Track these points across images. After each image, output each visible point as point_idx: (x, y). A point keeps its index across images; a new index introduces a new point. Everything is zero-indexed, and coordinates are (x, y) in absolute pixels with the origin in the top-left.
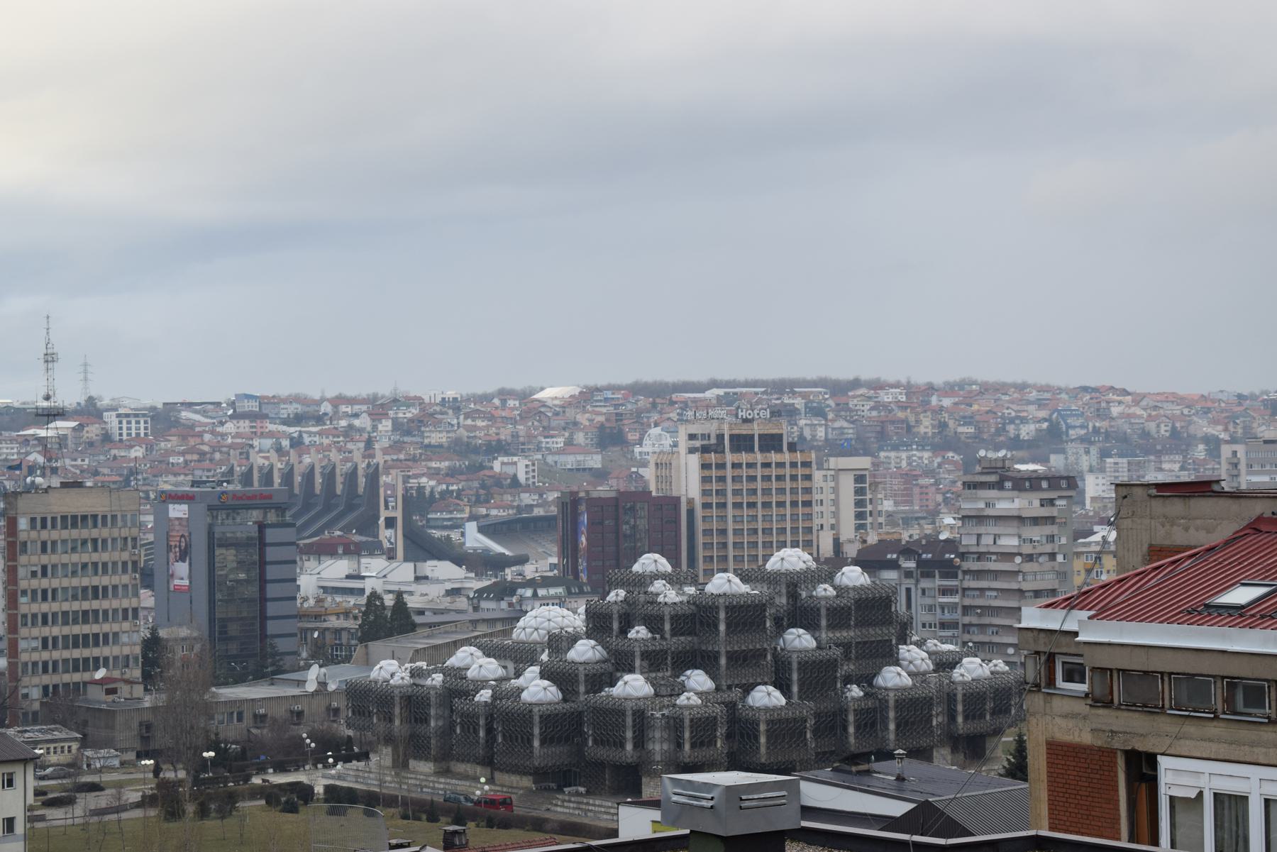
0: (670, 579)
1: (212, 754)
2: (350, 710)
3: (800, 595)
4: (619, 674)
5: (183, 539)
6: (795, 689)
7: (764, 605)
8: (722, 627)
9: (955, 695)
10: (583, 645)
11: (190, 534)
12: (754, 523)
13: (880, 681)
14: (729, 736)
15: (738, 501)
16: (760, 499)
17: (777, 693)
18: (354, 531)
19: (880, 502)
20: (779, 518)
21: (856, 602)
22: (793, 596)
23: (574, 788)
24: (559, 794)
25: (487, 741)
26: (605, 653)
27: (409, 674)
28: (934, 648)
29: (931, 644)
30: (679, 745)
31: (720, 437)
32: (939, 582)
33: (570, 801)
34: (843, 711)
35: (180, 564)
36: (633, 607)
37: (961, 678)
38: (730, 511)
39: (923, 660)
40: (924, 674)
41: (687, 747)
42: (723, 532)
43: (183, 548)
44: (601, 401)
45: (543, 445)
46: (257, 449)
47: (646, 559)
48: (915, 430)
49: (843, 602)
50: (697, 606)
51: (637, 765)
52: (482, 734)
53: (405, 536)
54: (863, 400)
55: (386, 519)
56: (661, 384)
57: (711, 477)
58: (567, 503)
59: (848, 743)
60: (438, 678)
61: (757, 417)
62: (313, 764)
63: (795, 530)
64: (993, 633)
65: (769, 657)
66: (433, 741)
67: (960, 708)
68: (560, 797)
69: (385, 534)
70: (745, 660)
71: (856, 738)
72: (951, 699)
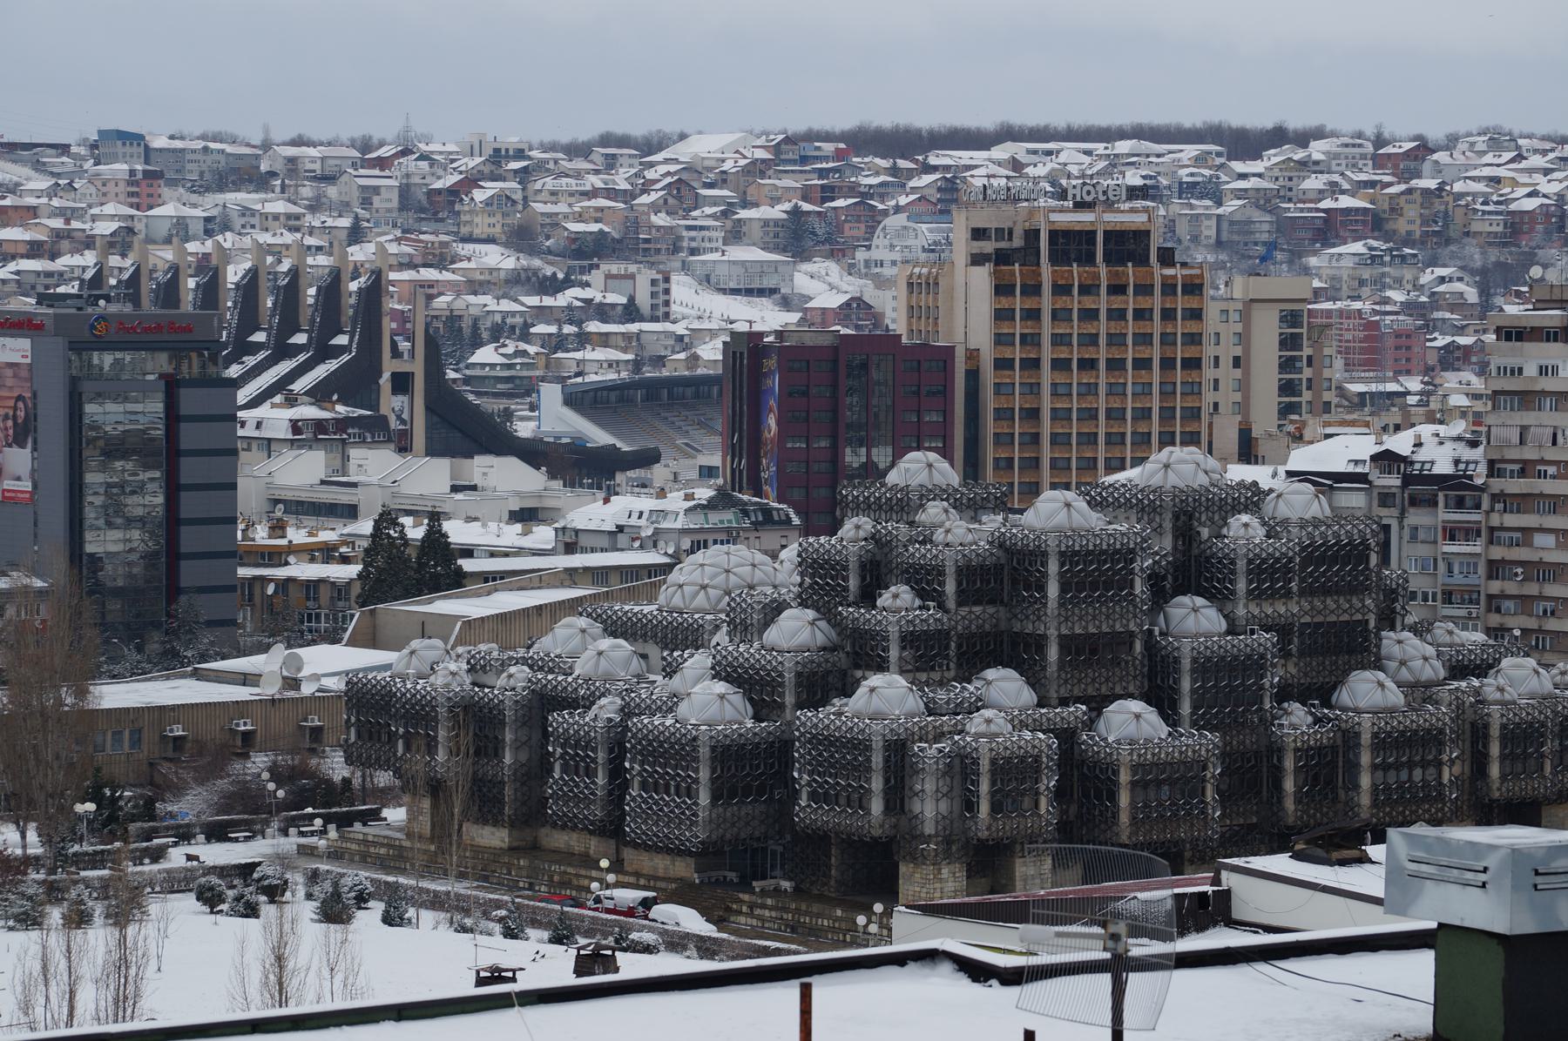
0: (956, 500)
1: (90, 807)
2: (353, 730)
3: (1198, 533)
4: (859, 674)
5: (21, 405)
6: (1186, 708)
7: (1132, 551)
8: (1053, 590)
9: (1486, 726)
10: (789, 618)
11: (35, 395)
12: (1090, 398)
13: (1344, 696)
14: (1060, 794)
15: (1062, 356)
16: (1103, 354)
17: (1151, 715)
18: (335, 397)
19: (1327, 360)
20: (1139, 389)
21: (1303, 549)
22: (1185, 532)
23: (773, 881)
24: (744, 892)
25: (610, 793)
26: (833, 634)
27: (465, 667)
28: (1447, 639)
29: (1440, 630)
30: (970, 806)
31: (1032, 235)
32: (1444, 515)
33: (764, 906)
34: (1276, 750)
35: (16, 450)
36: (886, 550)
37: (1498, 695)
38: (1047, 375)
39: (1426, 659)
40: (1428, 685)
41: (984, 808)
42: (1033, 414)
43: (20, 421)
44: (793, 162)
45: (685, 244)
46: (142, 236)
47: (910, 462)
48: (1390, 226)
49: (1280, 546)
50: (1007, 550)
51: (892, 839)
52: (601, 780)
53: (429, 409)
54: (1291, 169)
55: (394, 375)
56: (907, 131)
57: (1014, 310)
58: (741, 354)
59: (1282, 809)
60: (520, 673)
61: (1102, 198)
62: (280, 830)
63: (1167, 414)
64: (1545, 612)
65: (1138, 646)
66: (508, 791)
67: (1495, 750)
68: (746, 897)
69: (391, 404)
70: (1093, 652)
71: (1298, 801)
72: (1478, 733)
